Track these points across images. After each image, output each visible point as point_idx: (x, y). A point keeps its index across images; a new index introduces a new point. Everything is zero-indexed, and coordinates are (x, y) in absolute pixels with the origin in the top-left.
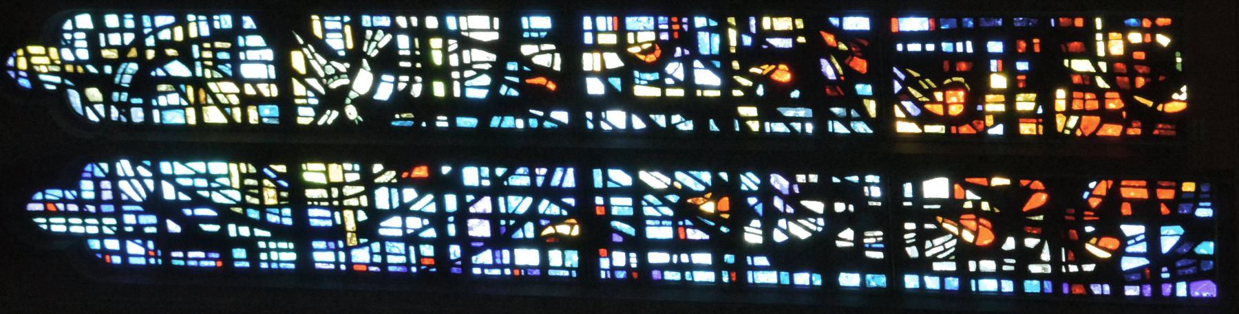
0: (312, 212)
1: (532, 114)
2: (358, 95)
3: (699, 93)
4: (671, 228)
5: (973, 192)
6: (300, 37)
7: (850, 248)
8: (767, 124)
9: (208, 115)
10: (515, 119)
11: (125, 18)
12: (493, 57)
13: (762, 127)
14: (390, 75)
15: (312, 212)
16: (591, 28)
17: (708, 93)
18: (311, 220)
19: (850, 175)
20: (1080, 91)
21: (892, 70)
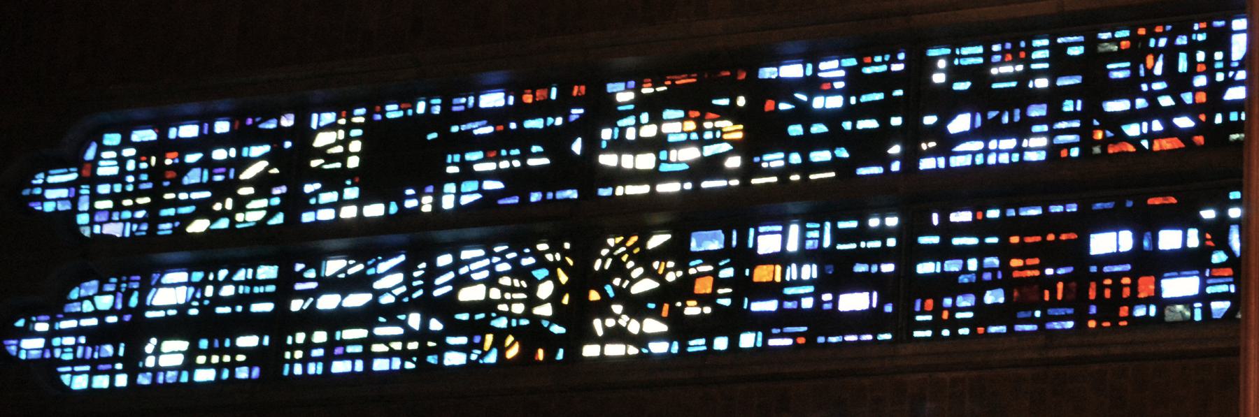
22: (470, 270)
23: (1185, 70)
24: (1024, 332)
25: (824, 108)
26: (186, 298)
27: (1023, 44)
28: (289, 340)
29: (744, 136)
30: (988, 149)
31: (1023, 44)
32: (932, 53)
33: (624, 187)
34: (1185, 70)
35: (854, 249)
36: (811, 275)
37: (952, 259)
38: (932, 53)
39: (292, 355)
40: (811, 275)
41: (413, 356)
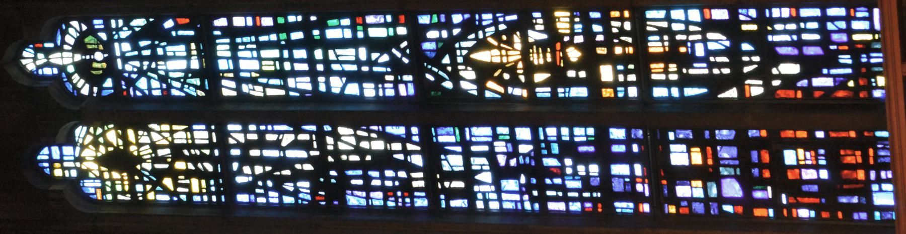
0: (537, 90)
1: (129, 57)
2: (342, 65)
3: (389, 18)
4: (572, 89)
5: (637, 92)
6: (497, 98)
7: (112, 94)
8: (560, 90)
9: (582, 93)
10: (229, 69)
11: (512, 94)
12: (549, 89)
13: (554, 93)
14: (531, 135)
15: (537, 90)
16: (162, 130)
17: (380, 19)
18: (223, 89)
19: (723, 91)
20: (691, 46)
21: (728, 57)
22: (505, 56)
23: (806, 132)
24: (200, 46)
25: (331, 87)
26: (469, 90)
27: (631, 67)
28: (141, 198)
29: (404, 97)
30: (279, 58)
31: (631, 67)
32: (769, 188)
33: (809, 216)
34: (806, 132)
35: (431, 81)
36: (227, 50)
37: (546, 97)
38: (769, 188)
39: (319, 62)
40: (227, 50)
41: (112, 33)
